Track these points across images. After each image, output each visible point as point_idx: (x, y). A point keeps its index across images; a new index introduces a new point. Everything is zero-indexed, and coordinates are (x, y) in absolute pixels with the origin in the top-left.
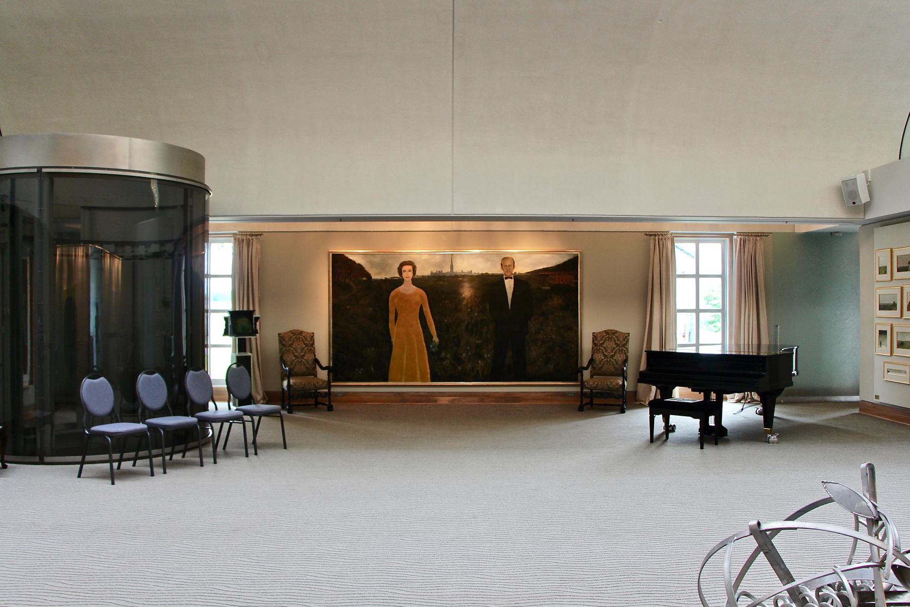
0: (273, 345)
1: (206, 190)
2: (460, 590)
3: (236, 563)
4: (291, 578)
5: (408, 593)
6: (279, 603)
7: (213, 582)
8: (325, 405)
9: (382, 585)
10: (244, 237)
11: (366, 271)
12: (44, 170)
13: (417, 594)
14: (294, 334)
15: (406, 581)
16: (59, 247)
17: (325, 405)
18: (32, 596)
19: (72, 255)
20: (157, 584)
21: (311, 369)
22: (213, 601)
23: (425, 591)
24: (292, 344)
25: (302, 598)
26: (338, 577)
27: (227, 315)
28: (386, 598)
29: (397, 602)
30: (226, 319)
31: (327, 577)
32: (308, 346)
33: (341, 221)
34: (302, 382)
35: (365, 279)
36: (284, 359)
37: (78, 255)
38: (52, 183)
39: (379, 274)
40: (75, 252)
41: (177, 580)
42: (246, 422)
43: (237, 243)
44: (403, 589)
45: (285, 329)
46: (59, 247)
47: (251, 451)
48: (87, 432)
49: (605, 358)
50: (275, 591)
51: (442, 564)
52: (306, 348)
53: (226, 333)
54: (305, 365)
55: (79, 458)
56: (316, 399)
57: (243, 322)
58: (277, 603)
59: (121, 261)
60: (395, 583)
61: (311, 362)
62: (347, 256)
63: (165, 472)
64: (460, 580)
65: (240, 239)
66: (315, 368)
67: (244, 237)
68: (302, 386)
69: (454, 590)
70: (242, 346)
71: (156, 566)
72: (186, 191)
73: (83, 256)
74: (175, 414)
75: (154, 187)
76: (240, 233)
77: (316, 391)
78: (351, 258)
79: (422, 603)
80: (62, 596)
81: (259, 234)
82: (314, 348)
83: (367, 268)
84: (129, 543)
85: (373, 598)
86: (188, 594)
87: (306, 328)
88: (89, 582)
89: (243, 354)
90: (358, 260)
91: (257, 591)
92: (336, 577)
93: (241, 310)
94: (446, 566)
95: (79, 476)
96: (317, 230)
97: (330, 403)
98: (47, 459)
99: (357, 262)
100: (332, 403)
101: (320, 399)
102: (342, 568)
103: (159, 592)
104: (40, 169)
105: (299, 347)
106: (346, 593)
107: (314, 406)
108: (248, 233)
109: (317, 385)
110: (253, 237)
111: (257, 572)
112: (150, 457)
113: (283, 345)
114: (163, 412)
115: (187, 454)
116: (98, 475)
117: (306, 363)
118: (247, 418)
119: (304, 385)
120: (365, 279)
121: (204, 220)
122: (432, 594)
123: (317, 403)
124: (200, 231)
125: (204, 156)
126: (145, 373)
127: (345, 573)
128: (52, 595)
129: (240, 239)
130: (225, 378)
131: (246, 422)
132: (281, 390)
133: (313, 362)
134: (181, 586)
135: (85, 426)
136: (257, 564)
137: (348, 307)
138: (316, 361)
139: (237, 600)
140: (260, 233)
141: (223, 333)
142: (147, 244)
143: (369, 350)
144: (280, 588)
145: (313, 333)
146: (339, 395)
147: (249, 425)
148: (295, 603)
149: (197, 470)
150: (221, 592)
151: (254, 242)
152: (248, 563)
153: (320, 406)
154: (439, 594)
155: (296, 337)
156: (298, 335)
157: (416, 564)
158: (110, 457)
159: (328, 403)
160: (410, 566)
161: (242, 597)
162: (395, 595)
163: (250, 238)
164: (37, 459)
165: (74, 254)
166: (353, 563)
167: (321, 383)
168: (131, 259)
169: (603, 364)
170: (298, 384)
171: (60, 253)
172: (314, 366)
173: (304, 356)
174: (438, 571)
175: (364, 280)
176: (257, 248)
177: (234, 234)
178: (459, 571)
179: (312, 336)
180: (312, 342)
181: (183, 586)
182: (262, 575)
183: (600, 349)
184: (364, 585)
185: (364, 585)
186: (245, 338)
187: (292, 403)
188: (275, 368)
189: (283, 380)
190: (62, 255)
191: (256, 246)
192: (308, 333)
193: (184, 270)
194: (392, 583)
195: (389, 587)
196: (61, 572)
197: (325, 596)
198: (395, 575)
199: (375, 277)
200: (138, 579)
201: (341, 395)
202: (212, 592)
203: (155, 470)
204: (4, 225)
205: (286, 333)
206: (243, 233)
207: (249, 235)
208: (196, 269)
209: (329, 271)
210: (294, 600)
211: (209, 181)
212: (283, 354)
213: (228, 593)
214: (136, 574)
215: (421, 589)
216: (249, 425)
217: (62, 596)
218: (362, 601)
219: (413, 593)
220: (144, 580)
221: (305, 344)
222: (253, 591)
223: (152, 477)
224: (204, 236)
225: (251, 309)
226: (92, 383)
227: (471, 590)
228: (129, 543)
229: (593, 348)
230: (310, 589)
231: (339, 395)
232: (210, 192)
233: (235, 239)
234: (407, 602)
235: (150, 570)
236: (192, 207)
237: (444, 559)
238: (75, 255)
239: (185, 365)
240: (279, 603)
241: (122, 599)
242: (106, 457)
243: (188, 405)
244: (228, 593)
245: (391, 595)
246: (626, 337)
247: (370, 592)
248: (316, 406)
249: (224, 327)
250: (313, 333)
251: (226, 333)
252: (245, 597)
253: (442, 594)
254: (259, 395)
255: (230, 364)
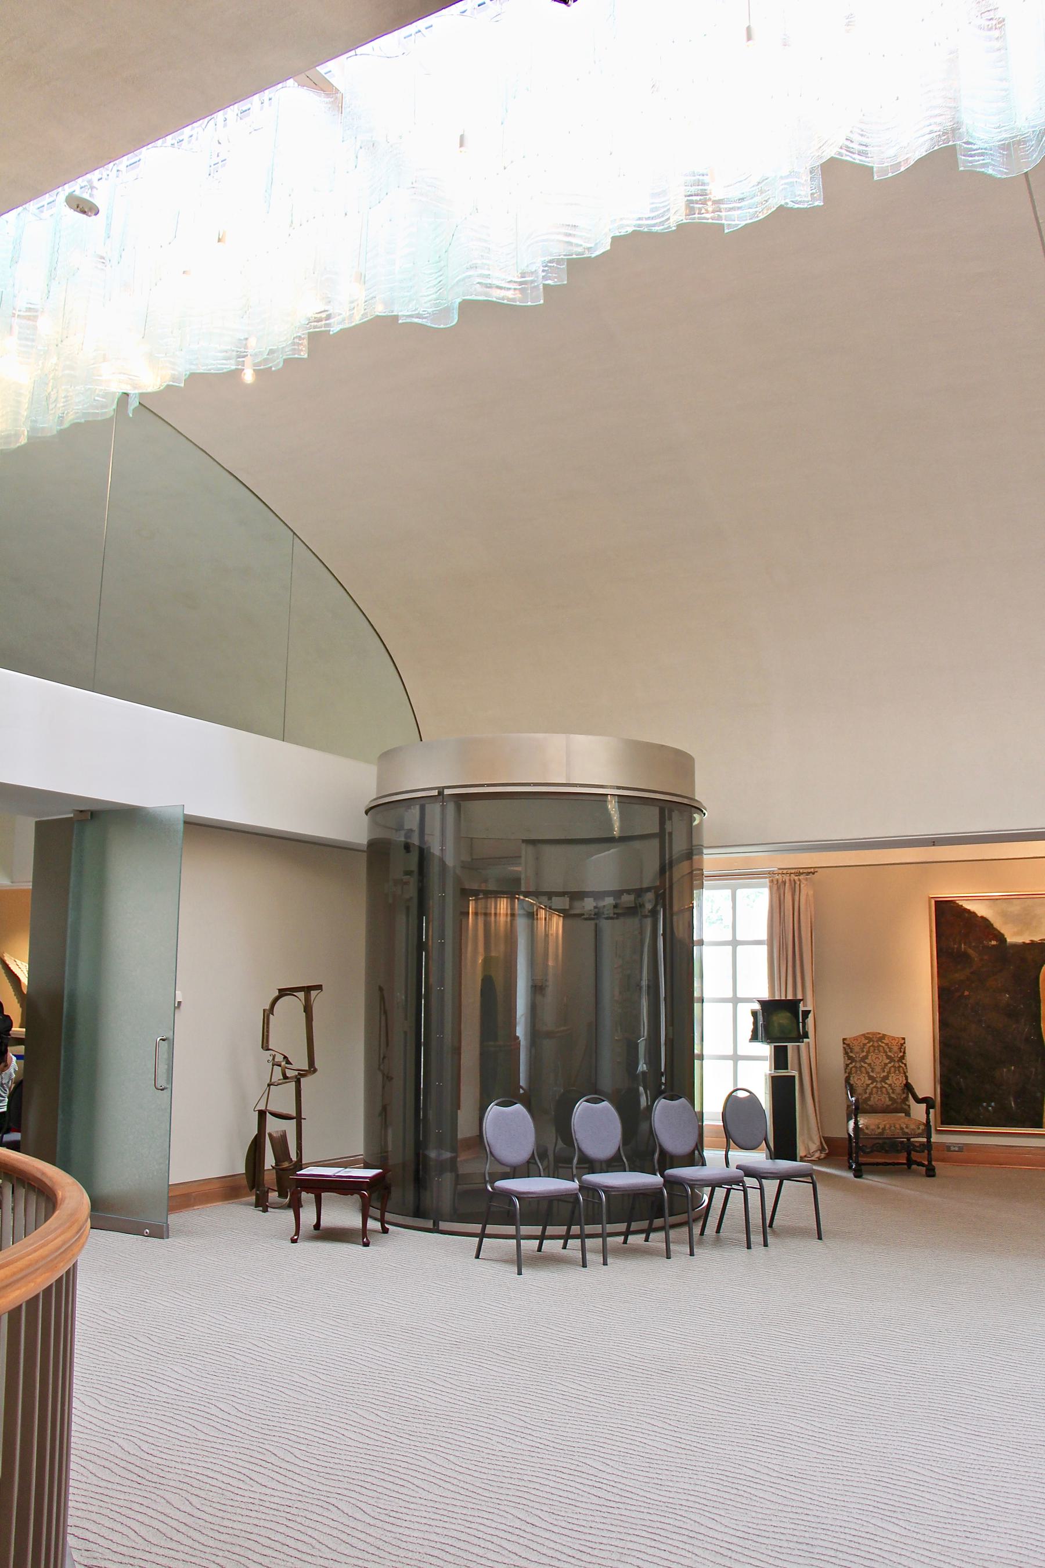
0: (836, 1060)
1: (695, 808)
2: (1011, 1549)
3: (639, 1426)
4: (715, 1466)
5: (904, 1532)
6: (672, 1506)
7: (587, 1451)
8: (923, 1165)
9: (866, 1508)
10: (787, 878)
11: (996, 929)
12: (447, 792)
13: (922, 1538)
14: (870, 1040)
15: (912, 1508)
16: (472, 900)
17: (923, 1165)
18: (329, 1427)
19: (491, 914)
20: (504, 1441)
21: (899, 1101)
22: (572, 1484)
23: (939, 1536)
24: (866, 1057)
25: (715, 1504)
26: (796, 1479)
27: (757, 1007)
28: (860, 1534)
29: (878, 1545)
30: (754, 1014)
31: (775, 1474)
32: (856, 1061)
33: (934, 845)
34: (879, 1124)
35: (994, 943)
36: (852, 1082)
37: (500, 914)
38: (458, 808)
39: (1019, 933)
40: (496, 908)
41: (535, 1439)
42: (748, 1189)
43: (775, 887)
44: (901, 1523)
45: (853, 1031)
46: (472, 900)
47: (757, 1238)
48: (490, 1189)
49: (872, 1083)
50: (677, 1485)
51: (999, 1489)
52: (890, 1065)
53: (754, 1037)
54: (888, 1093)
55: (477, 1228)
56: (909, 1154)
57: (782, 1018)
58: (669, 1505)
59: (561, 918)
60: (891, 1508)
61: (898, 1090)
62: (960, 903)
63: (605, 1263)
64: (1020, 1527)
65: (780, 881)
66: (906, 1099)
67: (787, 878)
68: (880, 1130)
69: (999, 1546)
70: (780, 1059)
71: (517, 1412)
72: (662, 812)
73: (507, 914)
74: (632, 1170)
75: (612, 807)
76: (780, 871)
77: (909, 1139)
78: (968, 907)
79: (922, 1559)
80: (367, 1433)
81: (811, 872)
82: (905, 1065)
83: (998, 924)
84: (496, 1369)
85: (838, 1529)
86: (540, 1466)
87: (892, 1029)
88: (412, 1420)
89: (782, 1073)
90: (980, 909)
91: (647, 1480)
92: (790, 1478)
93: (783, 998)
94: (1006, 1495)
95: (477, 1257)
96: (908, 861)
97: (930, 1162)
98: (443, 1225)
99: (979, 914)
100: (933, 1163)
101: (915, 1156)
102: (809, 1464)
103: (500, 1454)
104: (441, 791)
105: (878, 1062)
106: (794, 1510)
107: (906, 1166)
108: (793, 871)
109: (906, 1130)
110: (801, 877)
111: (664, 1447)
112: (582, 1237)
113: (850, 1058)
114: (613, 1164)
115: (652, 1236)
116: (505, 1258)
117: (891, 1091)
118: (750, 1182)
119: (884, 1129)
120: (994, 943)
121: (692, 853)
122: (950, 1545)
123: (910, 1163)
124: (687, 871)
125: (694, 756)
126: (586, 1101)
127: (812, 1473)
128: (355, 1429)
129: (780, 881)
130: (721, 1110)
131: (748, 1189)
132: (847, 1136)
133: (903, 1090)
134: (537, 1450)
135: (487, 1179)
136: (673, 1433)
137: (966, 993)
138: (908, 1088)
139: (609, 1489)
140: (812, 870)
141: (750, 1037)
142: (597, 895)
143: (1005, 1070)
144: (687, 1480)
145: (904, 1039)
146: (952, 1149)
147: (754, 1196)
148: (698, 1511)
149: (660, 1264)
150: (592, 1471)
151: (802, 886)
152: (658, 1430)
153: (914, 1167)
154: (965, 1547)
155: (872, 1046)
156: (875, 1041)
157: (948, 1479)
158: (518, 1230)
159: (926, 1163)
160: (936, 1482)
161: (620, 1486)
162: (880, 1532)
163: (796, 878)
164: (430, 1224)
165: (493, 912)
166: (834, 1458)
167: (912, 1126)
168: (593, 919)
169: (871, 1094)
170: (872, 1127)
171: (474, 911)
172: (904, 1096)
173: (888, 1079)
174: (985, 1500)
175: (993, 945)
176: (807, 895)
177: (773, 873)
178: (1026, 1509)
179: (902, 1045)
180: (901, 1054)
181: (539, 1450)
182: (670, 1454)
183: (862, 1066)
184: (832, 1502)
185: (832, 1502)
186: (787, 1046)
187: (862, 1160)
188: (840, 1098)
189: (849, 1119)
190: (476, 914)
191: (806, 891)
192: (894, 1038)
193: (662, 935)
194: (886, 1507)
195: (876, 1515)
196: (383, 1399)
197: (755, 1509)
198: (898, 1493)
199: (1011, 939)
200: (480, 1429)
201: (957, 1149)
202: (578, 1468)
203: (589, 1256)
204: (408, 873)
205: (855, 1039)
206: (785, 871)
207: (794, 873)
208: (680, 932)
209: (931, 931)
210: (700, 1506)
211: (701, 794)
212: (850, 1073)
213: (600, 1474)
214: (482, 1419)
215: (934, 1529)
216: (754, 1196)
217: (367, 1433)
218: (815, 1531)
219: (915, 1535)
220: (488, 1430)
221: (888, 1057)
222: (641, 1479)
223: (583, 1269)
224: (695, 879)
225: (799, 997)
226: (503, 1113)
227: (1032, 1554)
228: (496, 1369)
229: (847, 1065)
230: (735, 1491)
231: (952, 1149)
232: (704, 811)
233: (772, 881)
234: (896, 1550)
235: (504, 1417)
236: (670, 834)
237: (1008, 1480)
238: (495, 914)
239: (663, 1087)
240: (672, 1506)
241: (443, 1455)
242: (511, 1229)
243: (656, 1156)
244: (600, 1474)
245: (872, 1529)
246: (902, 1045)
247: (837, 1517)
248: (909, 1167)
249: (751, 1027)
250: (904, 1039)
251: (754, 1037)
252: (623, 1487)
253: (971, 1548)
254: (814, 1143)
255: (732, 1090)
